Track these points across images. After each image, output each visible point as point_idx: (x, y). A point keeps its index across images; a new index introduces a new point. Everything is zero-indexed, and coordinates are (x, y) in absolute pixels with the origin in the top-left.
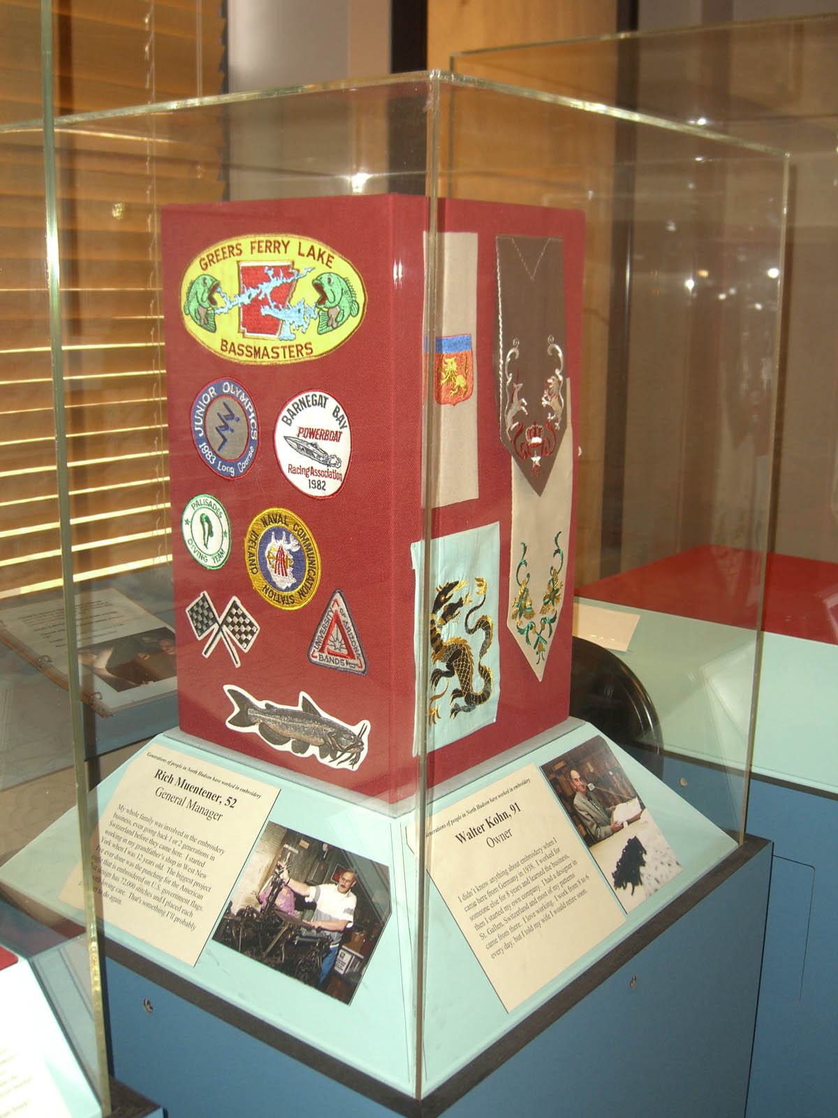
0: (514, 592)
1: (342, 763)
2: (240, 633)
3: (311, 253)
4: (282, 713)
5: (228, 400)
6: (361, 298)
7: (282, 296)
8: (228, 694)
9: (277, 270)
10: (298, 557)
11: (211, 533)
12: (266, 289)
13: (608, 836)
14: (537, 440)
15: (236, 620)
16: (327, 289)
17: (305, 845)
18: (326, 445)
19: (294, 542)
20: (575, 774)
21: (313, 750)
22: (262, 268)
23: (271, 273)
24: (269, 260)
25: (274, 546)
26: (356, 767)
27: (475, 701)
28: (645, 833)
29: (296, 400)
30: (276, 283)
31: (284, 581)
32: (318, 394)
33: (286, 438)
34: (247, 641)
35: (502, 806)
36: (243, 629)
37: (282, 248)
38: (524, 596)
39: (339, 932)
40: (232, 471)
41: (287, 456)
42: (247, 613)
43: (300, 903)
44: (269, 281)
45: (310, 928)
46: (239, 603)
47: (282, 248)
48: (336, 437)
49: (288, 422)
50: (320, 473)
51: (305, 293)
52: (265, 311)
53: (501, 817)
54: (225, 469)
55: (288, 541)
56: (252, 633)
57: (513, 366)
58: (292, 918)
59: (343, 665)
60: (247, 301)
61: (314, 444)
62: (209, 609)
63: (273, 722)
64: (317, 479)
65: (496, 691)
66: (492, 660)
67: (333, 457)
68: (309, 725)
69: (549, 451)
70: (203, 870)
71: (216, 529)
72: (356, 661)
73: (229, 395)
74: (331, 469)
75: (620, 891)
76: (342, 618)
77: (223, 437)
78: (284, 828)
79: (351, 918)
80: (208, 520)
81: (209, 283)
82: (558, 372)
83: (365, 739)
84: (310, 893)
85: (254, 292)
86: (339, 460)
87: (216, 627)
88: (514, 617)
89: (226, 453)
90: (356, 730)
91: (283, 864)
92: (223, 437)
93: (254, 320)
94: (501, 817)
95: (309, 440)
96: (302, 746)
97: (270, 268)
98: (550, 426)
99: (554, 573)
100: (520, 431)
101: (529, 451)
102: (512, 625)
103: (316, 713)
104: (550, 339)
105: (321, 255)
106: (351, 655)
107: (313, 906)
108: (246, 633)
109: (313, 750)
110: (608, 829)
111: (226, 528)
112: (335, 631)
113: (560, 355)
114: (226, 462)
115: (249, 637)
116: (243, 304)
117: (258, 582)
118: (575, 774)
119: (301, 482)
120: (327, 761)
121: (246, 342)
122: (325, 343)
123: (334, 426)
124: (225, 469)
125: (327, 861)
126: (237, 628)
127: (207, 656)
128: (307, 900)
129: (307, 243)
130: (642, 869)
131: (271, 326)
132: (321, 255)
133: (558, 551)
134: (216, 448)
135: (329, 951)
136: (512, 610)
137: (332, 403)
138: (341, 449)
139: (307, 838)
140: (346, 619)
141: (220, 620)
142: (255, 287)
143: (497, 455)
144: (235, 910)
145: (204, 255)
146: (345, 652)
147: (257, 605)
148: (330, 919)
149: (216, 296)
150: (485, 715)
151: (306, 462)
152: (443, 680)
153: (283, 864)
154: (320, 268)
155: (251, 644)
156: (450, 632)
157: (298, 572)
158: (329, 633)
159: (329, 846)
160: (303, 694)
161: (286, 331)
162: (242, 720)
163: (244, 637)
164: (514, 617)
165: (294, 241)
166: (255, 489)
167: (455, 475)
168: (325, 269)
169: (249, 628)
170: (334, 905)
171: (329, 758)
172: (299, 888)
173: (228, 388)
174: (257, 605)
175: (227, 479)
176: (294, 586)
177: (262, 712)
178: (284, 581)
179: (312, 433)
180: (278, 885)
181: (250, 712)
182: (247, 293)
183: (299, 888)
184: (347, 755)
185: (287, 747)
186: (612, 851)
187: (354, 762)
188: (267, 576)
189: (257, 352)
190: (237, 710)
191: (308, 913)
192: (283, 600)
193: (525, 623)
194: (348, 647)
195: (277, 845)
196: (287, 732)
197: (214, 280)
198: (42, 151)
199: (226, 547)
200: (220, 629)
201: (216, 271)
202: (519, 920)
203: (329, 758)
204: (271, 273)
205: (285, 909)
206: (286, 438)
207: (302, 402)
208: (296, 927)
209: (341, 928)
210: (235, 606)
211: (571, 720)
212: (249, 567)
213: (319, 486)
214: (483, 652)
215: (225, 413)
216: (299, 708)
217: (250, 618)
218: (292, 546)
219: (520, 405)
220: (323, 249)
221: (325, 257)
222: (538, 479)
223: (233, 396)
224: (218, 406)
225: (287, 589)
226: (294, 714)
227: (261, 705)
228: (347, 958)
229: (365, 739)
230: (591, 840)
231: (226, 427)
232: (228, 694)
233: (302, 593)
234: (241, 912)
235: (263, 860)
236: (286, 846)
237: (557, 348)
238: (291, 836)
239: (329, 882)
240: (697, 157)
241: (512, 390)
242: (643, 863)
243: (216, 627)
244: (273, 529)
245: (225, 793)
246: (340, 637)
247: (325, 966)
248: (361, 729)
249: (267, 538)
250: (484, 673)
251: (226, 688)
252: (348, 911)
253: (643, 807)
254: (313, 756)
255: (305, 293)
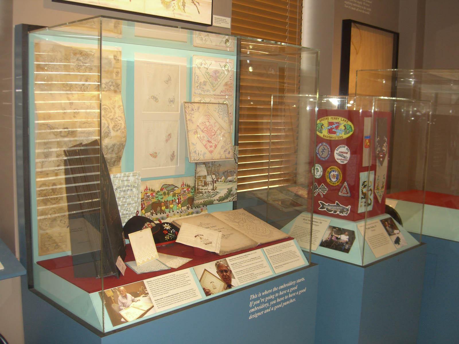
0: (376, 185)
1: (344, 214)
2: (323, 190)
3: (344, 120)
4: (331, 206)
5: (325, 146)
6: (353, 129)
7: (337, 127)
8: (320, 203)
9: (336, 123)
10: (337, 175)
11: (318, 171)
12: (334, 126)
13: (393, 235)
14: (381, 156)
15: (322, 188)
16: (346, 127)
17: (337, 229)
18: (345, 155)
19: (336, 172)
20: (386, 223)
21: (338, 212)
22: (333, 122)
23: (335, 123)
24: (334, 121)
25: (332, 173)
26: (347, 215)
27: (369, 205)
28: (401, 236)
29: (339, 146)
30: (336, 125)
31: (334, 180)
32: (344, 145)
33: (336, 153)
34: (325, 192)
35: (374, 225)
36: (324, 190)
37: (337, 119)
38: (378, 186)
39: (345, 242)
40: (324, 159)
41: (336, 157)
42: (325, 187)
43: (337, 238)
44: (334, 125)
45: (339, 242)
46: (323, 185)
47: (337, 119)
48: (347, 153)
49: (337, 150)
50: (343, 160)
51: (342, 127)
52: (333, 130)
53: (373, 227)
54: (322, 159)
55: (335, 172)
56: (326, 190)
57: (378, 142)
58: (336, 241)
59: (345, 195)
60: (329, 128)
61: (342, 154)
62: (317, 186)
63: (329, 208)
64: (342, 161)
65: (372, 204)
66: (372, 197)
67: (346, 157)
68: (338, 208)
69: (383, 158)
70: (316, 235)
71: (320, 171)
72: (348, 194)
73: (324, 145)
74: (346, 159)
75: (395, 245)
76: (346, 186)
77: (322, 153)
78: (332, 226)
79: (348, 240)
80: (318, 169)
81: (321, 124)
82: (386, 143)
83: (349, 209)
84: (339, 237)
85: (331, 127)
86: (347, 157)
87: (318, 190)
88: (376, 190)
89: (323, 156)
90: (347, 207)
91: (333, 232)
92: (322, 153)
93: (330, 131)
94: (373, 227)
95: (341, 154)
96: (335, 212)
97: (335, 122)
98: (384, 153)
99: (383, 182)
100: (378, 154)
101: (380, 157)
102: (376, 191)
103: (339, 205)
104: (384, 136)
105: (345, 121)
106: (347, 193)
107: (340, 238)
108: (325, 190)
109: (338, 212)
110: (393, 234)
111: (322, 170)
112: (344, 189)
113: (386, 140)
114: (323, 158)
115: (325, 191)
116: (329, 129)
117: (328, 180)
118: (386, 223)
119: (339, 162)
120: (341, 214)
121: (329, 135)
122: (345, 136)
123: (347, 151)
124: (322, 159)
125: (341, 231)
126: (323, 190)
127: (315, 196)
128: (339, 238)
129: (343, 119)
130: (400, 242)
131: (335, 133)
132: (345, 121)
133: (384, 178)
134: (321, 155)
135: (344, 245)
136: (376, 188)
137: (346, 147)
138: (348, 156)
139: (338, 228)
140: (347, 186)
141: (319, 188)
142: (331, 126)
143: (375, 157)
144: (324, 241)
145: (320, 119)
146: (346, 193)
147: (327, 185)
148: (343, 240)
149: (323, 127)
150: (370, 208)
151: (340, 158)
152: (363, 199)
153: (333, 232)
154: (345, 123)
155: (325, 193)
156: (365, 190)
157: (337, 178)
158: (343, 189)
159: (342, 229)
160: (336, 202)
161: (338, 134)
162: (323, 208)
163: (324, 191)
164: (376, 190)
165: (340, 118)
166: (329, 163)
167: (366, 162)
168: (346, 123)
169: (325, 190)
170: (344, 238)
171: (341, 213)
172: (337, 236)
173: (324, 144)
174: (327, 185)
175: (323, 161)
176: (336, 181)
177: (327, 206)
178: (334, 180)
179: (342, 152)
180: (332, 236)
181: (324, 206)
182: (330, 127)
183: (337, 236)
184: (345, 213)
185: (332, 212)
186: (394, 238)
187: (347, 214)
188: (330, 179)
189: (331, 137)
190: (321, 206)
191: (339, 240)
192: (334, 184)
193: (378, 191)
194: (347, 192)
195: (331, 229)
196: (332, 209)
197: (322, 124)
198: (132, 63)
199: (321, 174)
200: (319, 190)
201: (323, 122)
202: (377, 244)
203: (341, 213)
204: (335, 123)
205: (334, 239)
206: (336, 153)
207: (340, 147)
208: (337, 242)
209: (346, 241)
210: (323, 185)
211: (385, 214)
212: (326, 178)
213: (343, 162)
214: (370, 195)
215: (323, 148)
216: (336, 204)
217: (326, 187)
218: (336, 173)
219: (379, 149)
220: (346, 120)
221: (346, 121)
222: (381, 163)
223: (325, 145)
224: (322, 147)
225: (335, 181)
226: (334, 206)
227: (327, 204)
228: (347, 246)
229: (349, 209)
230: (390, 235)
231: (323, 151)
232: (320, 203)
233: (338, 182)
234: (325, 241)
235: (329, 232)
236: (333, 229)
237: (386, 138)
238: (334, 228)
239: (343, 234)
240: (415, 108)
241: (377, 146)
242: (400, 241)
243: (318, 190)
244: (332, 170)
245: (319, 221)
246: (345, 190)
247: (343, 248)
248: (349, 207)
249: (331, 172)
250: (370, 200)
251: (319, 202)
252: (347, 239)
253: (400, 232)
254: (338, 214)
255: (342, 127)
